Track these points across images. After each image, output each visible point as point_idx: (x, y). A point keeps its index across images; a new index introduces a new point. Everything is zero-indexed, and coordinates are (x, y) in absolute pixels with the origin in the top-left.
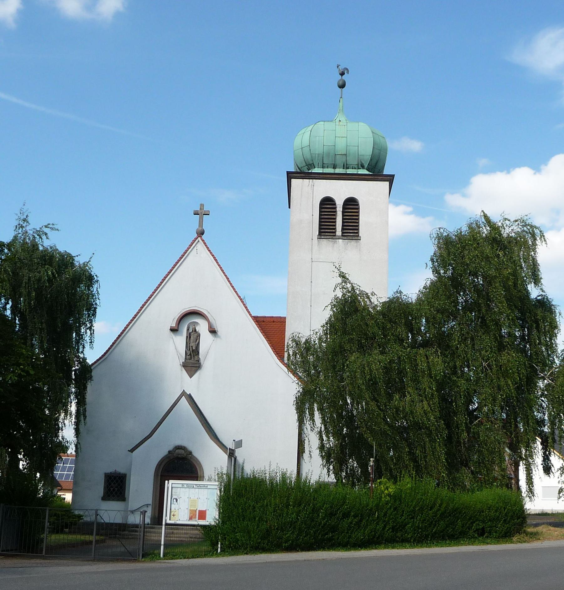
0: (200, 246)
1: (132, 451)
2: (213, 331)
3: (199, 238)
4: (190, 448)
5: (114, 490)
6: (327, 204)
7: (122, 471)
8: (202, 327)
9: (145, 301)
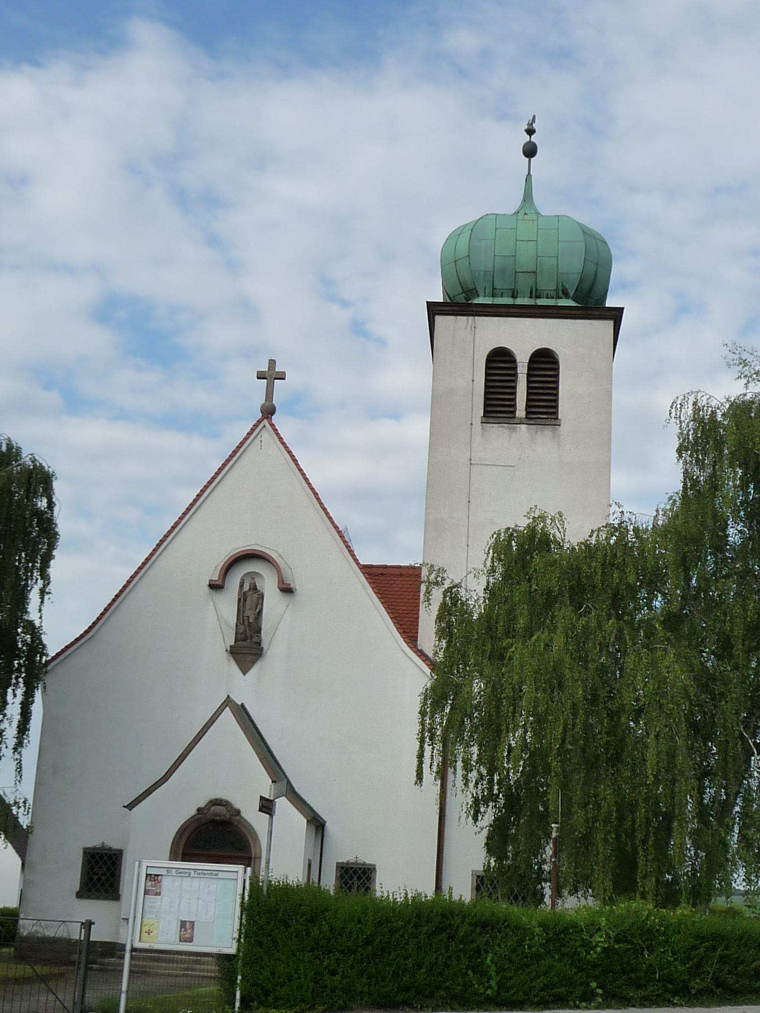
0: (266, 435)
2: (287, 590)
3: (265, 422)
5: (99, 879)
6: (500, 361)
8: (269, 586)
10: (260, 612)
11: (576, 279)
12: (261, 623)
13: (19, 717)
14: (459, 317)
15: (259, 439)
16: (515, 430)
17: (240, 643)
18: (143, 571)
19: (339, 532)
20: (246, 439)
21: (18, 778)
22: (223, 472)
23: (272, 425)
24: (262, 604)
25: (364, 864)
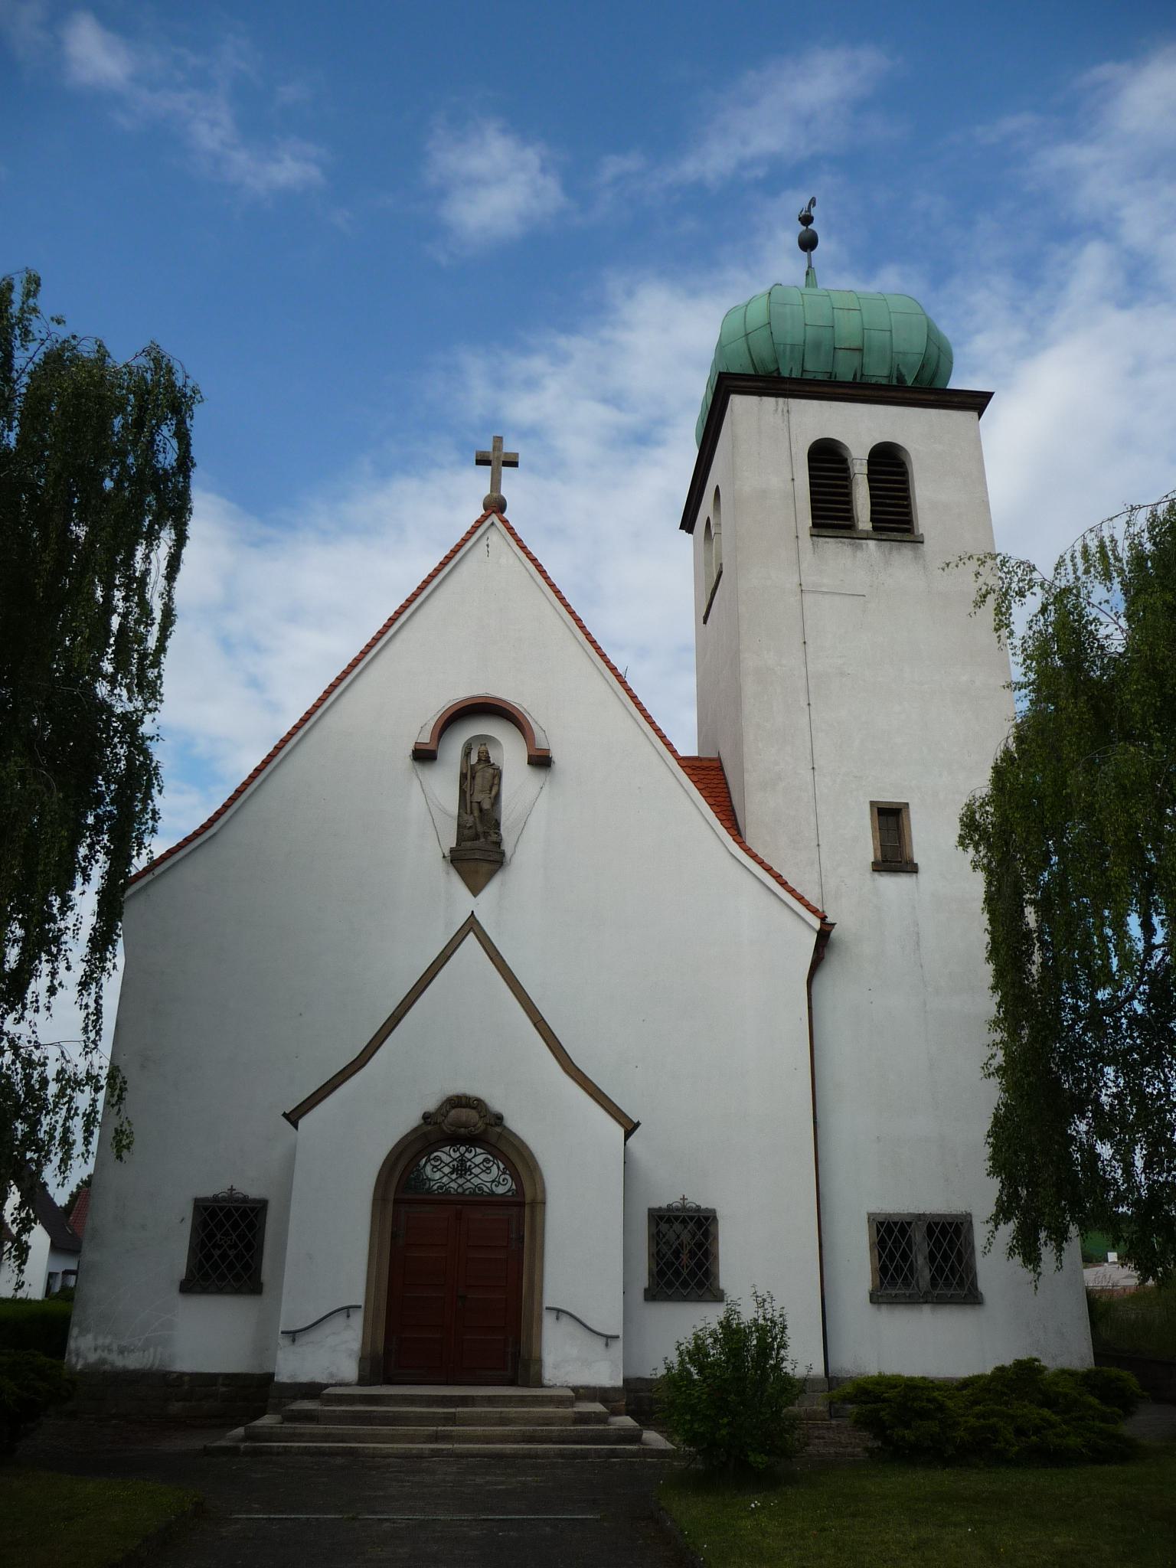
0: (496, 538)
1: (293, 1117)
2: (541, 761)
3: (494, 518)
4: (497, 1103)
5: (224, 1256)
6: (826, 457)
7: (251, 1189)
8: (510, 754)
9: (408, 595)
10: (498, 795)
11: (916, 360)
12: (500, 813)
13: (94, 920)
14: (765, 399)
15: (484, 542)
16: (859, 547)
17: (469, 844)
18: (301, 732)
19: (618, 676)
20: (465, 540)
21: (92, 1035)
22: (419, 600)
23: (505, 522)
24: (499, 784)
25: (698, 1209)
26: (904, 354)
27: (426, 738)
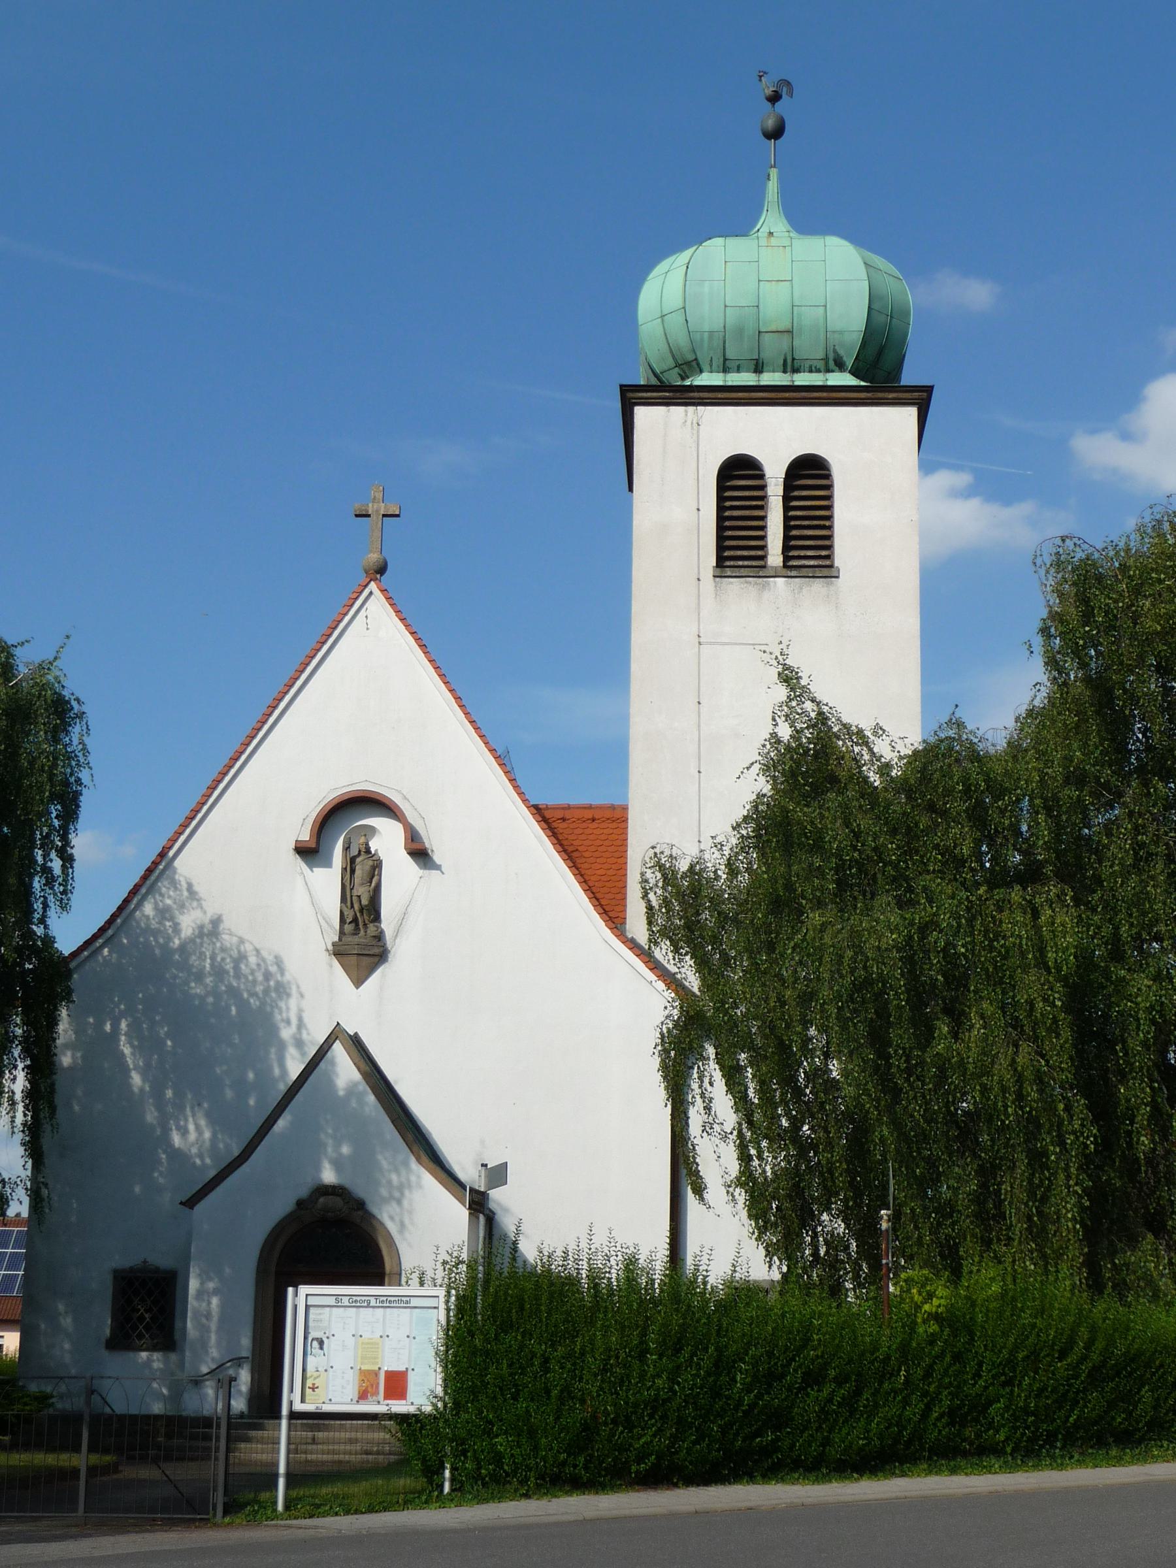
1: (191, 1203)
2: (420, 854)
6: (739, 473)
8: (387, 839)
14: (672, 408)
15: (363, 613)
24: (380, 875)
26: (841, 332)
27: (305, 836)
